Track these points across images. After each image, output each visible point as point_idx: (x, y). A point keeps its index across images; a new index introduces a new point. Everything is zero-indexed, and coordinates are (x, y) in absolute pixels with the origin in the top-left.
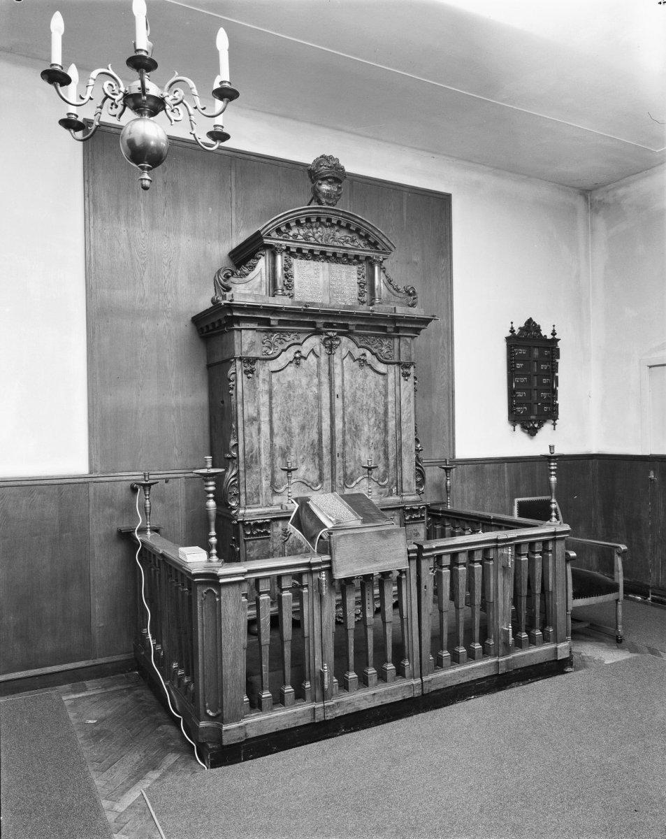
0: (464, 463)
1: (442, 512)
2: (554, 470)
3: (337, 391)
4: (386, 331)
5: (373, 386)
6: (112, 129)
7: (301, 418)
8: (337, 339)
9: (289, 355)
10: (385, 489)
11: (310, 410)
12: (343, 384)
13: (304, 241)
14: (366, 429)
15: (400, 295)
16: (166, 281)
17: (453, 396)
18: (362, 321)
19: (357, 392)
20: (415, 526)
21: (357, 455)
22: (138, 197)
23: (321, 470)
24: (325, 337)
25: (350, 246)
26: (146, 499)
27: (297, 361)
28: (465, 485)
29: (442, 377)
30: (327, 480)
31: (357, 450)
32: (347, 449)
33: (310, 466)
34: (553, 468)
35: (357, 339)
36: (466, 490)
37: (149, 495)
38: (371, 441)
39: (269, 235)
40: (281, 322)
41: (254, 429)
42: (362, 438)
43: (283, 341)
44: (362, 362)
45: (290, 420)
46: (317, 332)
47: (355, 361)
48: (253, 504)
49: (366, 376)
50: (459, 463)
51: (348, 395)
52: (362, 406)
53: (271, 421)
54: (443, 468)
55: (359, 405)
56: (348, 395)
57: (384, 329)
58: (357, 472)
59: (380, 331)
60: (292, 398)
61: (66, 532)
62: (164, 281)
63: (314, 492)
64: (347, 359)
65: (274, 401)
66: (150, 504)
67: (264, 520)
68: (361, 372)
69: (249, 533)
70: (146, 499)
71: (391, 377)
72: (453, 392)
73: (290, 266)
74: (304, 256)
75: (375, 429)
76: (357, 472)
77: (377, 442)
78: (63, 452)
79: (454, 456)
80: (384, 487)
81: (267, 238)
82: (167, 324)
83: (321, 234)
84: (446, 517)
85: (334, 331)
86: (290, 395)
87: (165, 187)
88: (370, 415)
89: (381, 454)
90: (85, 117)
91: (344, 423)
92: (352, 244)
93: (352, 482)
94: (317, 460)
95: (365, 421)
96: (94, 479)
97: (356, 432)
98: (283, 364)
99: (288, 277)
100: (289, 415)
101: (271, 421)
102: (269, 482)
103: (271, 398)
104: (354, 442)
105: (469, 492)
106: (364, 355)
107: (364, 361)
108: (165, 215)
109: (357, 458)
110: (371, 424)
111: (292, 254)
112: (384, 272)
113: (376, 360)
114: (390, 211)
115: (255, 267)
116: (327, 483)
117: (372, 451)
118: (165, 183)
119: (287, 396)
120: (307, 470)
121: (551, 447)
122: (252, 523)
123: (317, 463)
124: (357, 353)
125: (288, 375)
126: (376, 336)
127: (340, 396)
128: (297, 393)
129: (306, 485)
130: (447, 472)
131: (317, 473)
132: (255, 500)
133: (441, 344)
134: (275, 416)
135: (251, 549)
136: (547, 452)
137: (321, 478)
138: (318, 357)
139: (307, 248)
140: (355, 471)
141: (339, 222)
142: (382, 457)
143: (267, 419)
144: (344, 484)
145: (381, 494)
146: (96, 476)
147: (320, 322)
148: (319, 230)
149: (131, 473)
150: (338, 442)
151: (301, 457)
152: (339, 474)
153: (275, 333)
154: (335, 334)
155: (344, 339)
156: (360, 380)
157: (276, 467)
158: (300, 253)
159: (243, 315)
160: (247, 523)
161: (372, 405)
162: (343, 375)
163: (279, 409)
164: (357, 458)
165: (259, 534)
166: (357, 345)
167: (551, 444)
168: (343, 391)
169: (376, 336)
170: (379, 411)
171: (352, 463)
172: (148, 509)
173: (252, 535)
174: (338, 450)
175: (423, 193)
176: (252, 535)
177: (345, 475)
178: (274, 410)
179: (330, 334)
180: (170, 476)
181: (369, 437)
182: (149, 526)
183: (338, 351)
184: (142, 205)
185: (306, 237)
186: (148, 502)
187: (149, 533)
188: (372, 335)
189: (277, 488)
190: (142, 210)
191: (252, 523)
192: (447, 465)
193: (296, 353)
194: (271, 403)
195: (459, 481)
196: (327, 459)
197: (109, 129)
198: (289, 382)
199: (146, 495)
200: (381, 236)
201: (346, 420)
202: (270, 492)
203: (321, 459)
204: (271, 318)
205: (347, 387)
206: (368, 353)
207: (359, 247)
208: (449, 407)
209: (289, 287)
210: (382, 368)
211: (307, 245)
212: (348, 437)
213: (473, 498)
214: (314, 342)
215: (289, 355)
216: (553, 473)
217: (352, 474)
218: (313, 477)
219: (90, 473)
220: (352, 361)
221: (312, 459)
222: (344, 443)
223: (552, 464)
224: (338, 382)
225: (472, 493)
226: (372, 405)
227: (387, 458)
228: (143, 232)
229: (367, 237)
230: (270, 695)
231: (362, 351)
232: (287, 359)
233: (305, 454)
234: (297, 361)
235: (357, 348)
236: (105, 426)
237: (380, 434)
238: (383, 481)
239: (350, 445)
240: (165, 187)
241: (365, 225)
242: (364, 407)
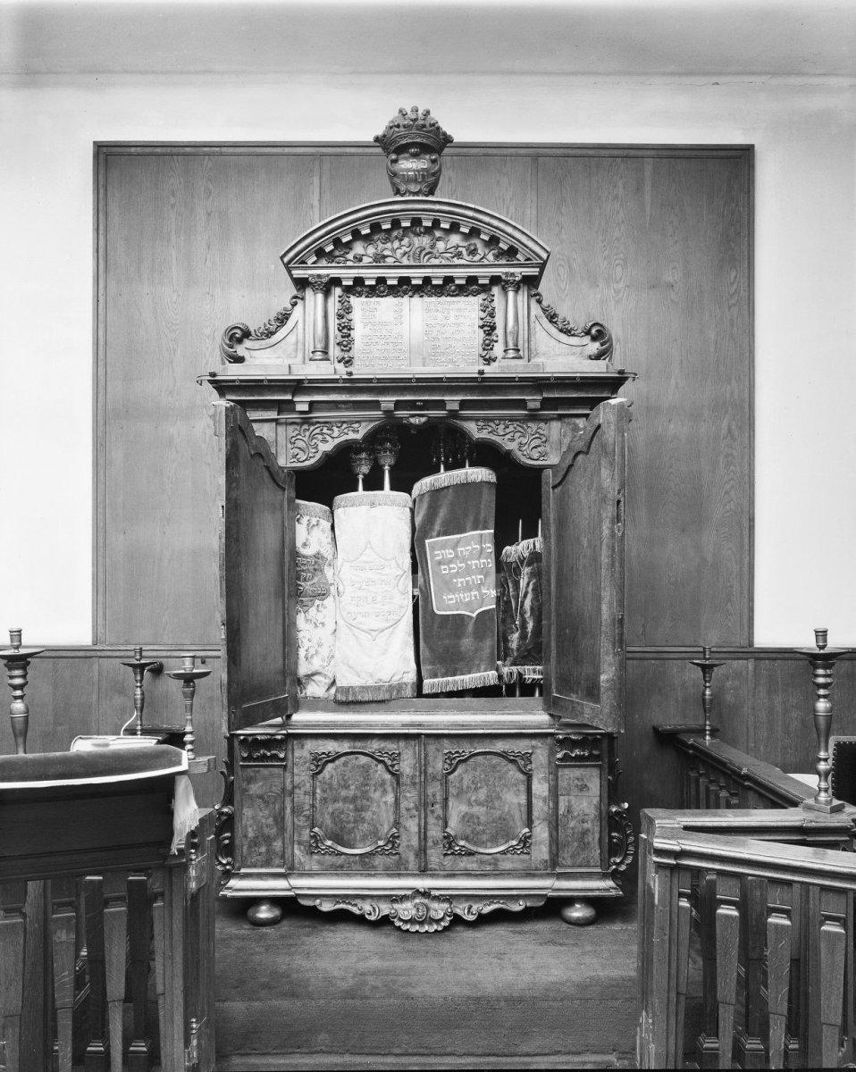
1: (692, 747)
2: (825, 686)
4: (525, 408)
6: (133, 150)
13: (374, 264)
16: (207, 363)
17: (752, 528)
22: (169, 241)
28: (778, 700)
34: (821, 680)
36: (779, 708)
43: (328, 438)
50: (762, 655)
57: (521, 404)
59: (517, 409)
62: (205, 361)
66: (143, 694)
72: (752, 520)
73: (348, 310)
74: (373, 291)
78: (61, 617)
79: (751, 644)
83: (408, 250)
96: (99, 654)
111: (348, 290)
112: (539, 302)
114: (616, 197)
115: (287, 319)
121: (822, 635)
122: (250, 739)
126: (512, 419)
130: (704, 673)
133: (724, 432)
136: (808, 643)
148: (403, 243)
149: (156, 647)
153: (313, 424)
158: (358, 287)
159: (475, 398)
165: (264, 758)
167: (821, 627)
172: (139, 702)
173: (249, 758)
180: (210, 653)
184: (174, 253)
185: (379, 259)
186: (138, 691)
188: (502, 419)
192: (705, 658)
195: (762, 691)
197: (128, 150)
208: (742, 546)
211: (440, 270)
213: (795, 725)
216: (822, 692)
219: (95, 643)
223: (821, 672)
230: (145, 1049)
236: (117, 573)
241: (487, 219)
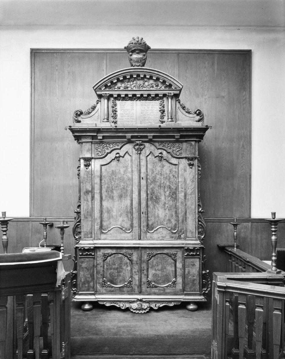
0: (258, 221)
1: (230, 252)
3: (143, 175)
5: (168, 172)
7: (119, 191)
8: (141, 145)
9: (113, 155)
10: (175, 235)
11: (126, 187)
12: (147, 172)
13: (124, 90)
14: (163, 198)
15: (191, 115)
18: (152, 133)
19: (157, 175)
20: (192, 260)
21: (156, 214)
22: (56, 81)
23: (132, 221)
24: (134, 144)
25: (155, 89)
26: (235, 232)
27: (118, 158)
28: (259, 236)
29: (242, 166)
30: (135, 227)
31: (157, 211)
32: (149, 210)
33: (125, 219)
35: (157, 144)
36: (259, 239)
37: (46, 229)
38: (167, 205)
39: (101, 89)
40: (104, 137)
41: (89, 197)
42: (160, 204)
43: (109, 148)
44: (161, 158)
45: (113, 192)
46: (129, 142)
47: (155, 157)
48: (88, 238)
49: (163, 166)
51: (151, 178)
52: (160, 184)
53: (101, 193)
54: (42, 224)
55: (158, 183)
56: (151, 178)
57: (173, 137)
58: (156, 223)
60: (114, 180)
61: (19, 244)
62: (67, 122)
63: (127, 234)
64: (150, 156)
65: (103, 181)
66: (46, 233)
67: (90, 247)
68: (160, 164)
69: (81, 254)
70: (235, 232)
71: (181, 166)
72: (250, 176)
73: (116, 105)
75: (169, 198)
76: (156, 223)
77: (171, 206)
79: (250, 217)
80: (175, 233)
81: (99, 91)
82: (69, 144)
84: (234, 256)
85: (140, 140)
86: (113, 178)
87: (69, 75)
88: (166, 190)
89: (174, 213)
90: (31, 48)
91: (147, 194)
92: (156, 88)
93: (153, 229)
94: (129, 215)
95: (163, 193)
96: (32, 220)
97: (157, 200)
98: (109, 161)
99: (115, 112)
100: (112, 189)
101: (101, 193)
102: (99, 226)
103: (101, 180)
104: (154, 206)
105: (262, 240)
106: (161, 153)
107: (162, 157)
108: (69, 89)
109: (156, 215)
110: (167, 195)
112: (179, 102)
113: (170, 156)
116: (136, 229)
117: (167, 211)
118: (69, 73)
119: (112, 178)
120: (123, 221)
121: (274, 214)
122: (82, 248)
123: (129, 217)
124: (157, 153)
125: (112, 167)
127: (145, 178)
128: (117, 177)
129: (122, 229)
130: (234, 227)
131: (130, 223)
132: (89, 236)
134: (104, 190)
135: (82, 262)
136: (269, 217)
137: (132, 226)
138: (131, 156)
139: (146, 93)
140: (154, 223)
141: (145, 76)
142: (174, 215)
143: (98, 191)
144: (147, 230)
145: (172, 237)
146: (32, 218)
147: (129, 135)
150: (143, 205)
151: (120, 213)
152: (144, 224)
154: (140, 142)
155: (147, 145)
156: (159, 169)
157: (104, 218)
158: (119, 97)
160: (80, 248)
161: (168, 184)
162: (147, 166)
163: (106, 186)
164: (156, 215)
166: (156, 148)
167: (274, 212)
168: (147, 175)
169: (170, 142)
170: (172, 187)
171: (153, 218)
173: (82, 255)
174: (143, 209)
175: (229, 53)
176: (82, 255)
177: (148, 225)
178: (103, 187)
179: (138, 142)
181: (165, 203)
182: (45, 245)
183: (143, 151)
186: (45, 232)
187: (235, 248)
188: (167, 141)
189: (104, 230)
190: (57, 89)
191: (82, 248)
193: (116, 154)
194: (101, 182)
196: (135, 215)
197: (41, 51)
198: (113, 171)
199: (235, 230)
200: (172, 80)
201: (149, 192)
202: (99, 232)
203: (132, 215)
204: (126, 135)
205: (150, 172)
206: (165, 153)
207: (162, 90)
209: (115, 116)
210: (174, 161)
212: (150, 203)
214: (129, 147)
215: (113, 155)
217: (152, 224)
218: (127, 225)
219: (30, 216)
220: (153, 157)
221: (127, 215)
222: (147, 206)
223: (273, 226)
224: (143, 170)
225: (264, 241)
226: (168, 184)
227: (177, 216)
228: (57, 99)
229: (164, 82)
231: (160, 151)
232: (111, 158)
233: (122, 212)
234: (118, 158)
235: (156, 149)
236: (37, 195)
237: (173, 201)
238: (174, 230)
239: (152, 207)
240: (69, 75)
242: (162, 185)
